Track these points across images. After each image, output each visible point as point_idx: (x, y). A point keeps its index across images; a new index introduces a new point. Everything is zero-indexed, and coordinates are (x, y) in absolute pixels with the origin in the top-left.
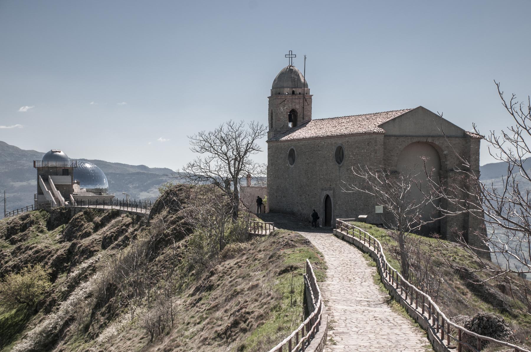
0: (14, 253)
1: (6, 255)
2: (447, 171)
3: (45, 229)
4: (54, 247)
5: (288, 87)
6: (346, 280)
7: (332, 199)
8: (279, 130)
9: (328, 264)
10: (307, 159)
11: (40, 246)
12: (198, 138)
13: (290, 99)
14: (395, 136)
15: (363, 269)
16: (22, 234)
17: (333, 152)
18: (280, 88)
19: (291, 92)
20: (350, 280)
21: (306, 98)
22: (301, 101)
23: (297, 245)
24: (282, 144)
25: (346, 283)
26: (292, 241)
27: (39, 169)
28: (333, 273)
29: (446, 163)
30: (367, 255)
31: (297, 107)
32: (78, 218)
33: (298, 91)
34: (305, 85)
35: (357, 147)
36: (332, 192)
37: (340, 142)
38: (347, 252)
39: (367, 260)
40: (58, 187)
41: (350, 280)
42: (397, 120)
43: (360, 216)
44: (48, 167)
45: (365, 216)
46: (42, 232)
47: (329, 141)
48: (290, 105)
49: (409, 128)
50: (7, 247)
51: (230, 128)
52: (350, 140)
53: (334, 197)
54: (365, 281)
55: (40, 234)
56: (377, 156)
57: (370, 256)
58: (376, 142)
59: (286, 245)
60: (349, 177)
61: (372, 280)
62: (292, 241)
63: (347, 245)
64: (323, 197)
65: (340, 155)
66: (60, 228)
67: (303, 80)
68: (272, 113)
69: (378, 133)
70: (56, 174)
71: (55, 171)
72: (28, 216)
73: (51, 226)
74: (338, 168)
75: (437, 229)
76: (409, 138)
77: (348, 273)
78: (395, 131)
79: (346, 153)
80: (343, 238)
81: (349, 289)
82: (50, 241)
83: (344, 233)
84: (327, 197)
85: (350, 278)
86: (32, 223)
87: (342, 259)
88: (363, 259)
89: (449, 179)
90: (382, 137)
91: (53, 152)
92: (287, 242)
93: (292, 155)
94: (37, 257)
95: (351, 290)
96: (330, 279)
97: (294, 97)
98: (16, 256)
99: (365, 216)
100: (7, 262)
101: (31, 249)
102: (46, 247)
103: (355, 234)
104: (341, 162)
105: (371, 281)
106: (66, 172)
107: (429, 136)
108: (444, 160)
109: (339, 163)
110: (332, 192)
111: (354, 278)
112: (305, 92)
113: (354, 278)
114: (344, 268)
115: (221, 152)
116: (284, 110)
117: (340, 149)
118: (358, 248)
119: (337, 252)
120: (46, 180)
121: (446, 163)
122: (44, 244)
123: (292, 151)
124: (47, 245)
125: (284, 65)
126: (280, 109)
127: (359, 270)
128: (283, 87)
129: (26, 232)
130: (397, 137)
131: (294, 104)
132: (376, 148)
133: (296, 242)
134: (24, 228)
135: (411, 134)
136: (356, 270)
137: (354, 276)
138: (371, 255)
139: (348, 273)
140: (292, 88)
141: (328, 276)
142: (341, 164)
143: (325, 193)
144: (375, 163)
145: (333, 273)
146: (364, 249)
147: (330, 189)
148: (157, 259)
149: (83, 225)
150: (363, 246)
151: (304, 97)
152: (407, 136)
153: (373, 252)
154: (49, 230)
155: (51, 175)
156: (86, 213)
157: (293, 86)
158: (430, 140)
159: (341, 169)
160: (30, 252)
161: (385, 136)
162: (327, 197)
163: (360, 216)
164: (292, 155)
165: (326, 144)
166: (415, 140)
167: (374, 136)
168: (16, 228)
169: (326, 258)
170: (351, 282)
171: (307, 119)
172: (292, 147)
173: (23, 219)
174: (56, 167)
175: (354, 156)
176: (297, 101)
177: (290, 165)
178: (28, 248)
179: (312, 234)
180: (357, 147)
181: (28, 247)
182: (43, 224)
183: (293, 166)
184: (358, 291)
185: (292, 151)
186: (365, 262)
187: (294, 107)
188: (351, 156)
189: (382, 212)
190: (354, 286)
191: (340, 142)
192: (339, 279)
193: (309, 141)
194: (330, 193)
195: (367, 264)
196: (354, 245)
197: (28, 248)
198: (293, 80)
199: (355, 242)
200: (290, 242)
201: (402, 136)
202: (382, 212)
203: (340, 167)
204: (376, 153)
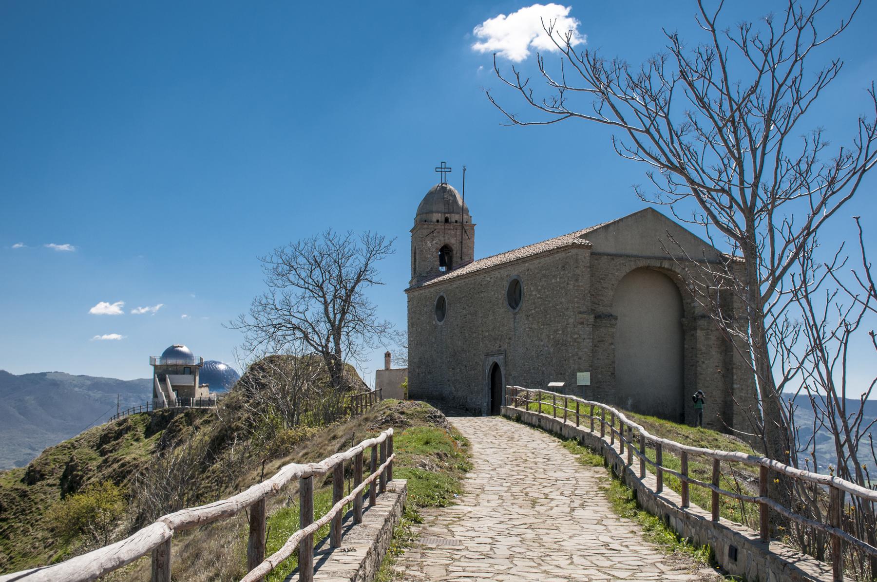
0: (99, 468)
1: (90, 470)
2: (695, 319)
3: (142, 436)
4: (143, 459)
5: (438, 212)
6: (520, 501)
7: (502, 369)
8: (425, 275)
9: (477, 461)
10: (464, 308)
11: (128, 458)
12: (275, 259)
13: (442, 230)
14: (608, 255)
15: (569, 472)
16: (115, 443)
17: (504, 292)
18: (426, 213)
19: (443, 220)
20: (534, 503)
21: (466, 228)
22: (459, 232)
23: (412, 422)
24: (427, 291)
25: (520, 511)
26: (402, 413)
27: (155, 366)
28: (485, 481)
29: (692, 305)
30: (572, 443)
31: (453, 241)
32: (176, 421)
33: (454, 217)
34: (464, 210)
35: (544, 276)
36: (502, 357)
37: (514, 272)
38: (525, 438)
39: (574, 452)
40: (175, 388)
41: (534, 503)
42: (611, 228)
43: (551, 384)
44: (167, 365)
45: (561, 384)
46: (137, 440)
47: (497, 274)
48: (442, 239)
49: (632, 243)
50: (95, 459)
51: (329, 243)
52: (531, 267)
53: (506, 363)
54: (582, 506)
55: (135, 443)
56: (579, 286)
57: (581, 443)
58: (577, 261)
59: (387, 422)
60: (531, 328)
61: (605, 502)
62: (402, 413)
63: (525, 430)
64: (488, 367)
65: (515, 294)
66: (157, 435)
67: (460, 203)
68: (415, 253)
69: (580, 246)
70: (176, 372)
71: (176, 370)
72: (125, 420)
73: (149, 433)
74: (512, 316)
75: (682, 410)
76: (633, 259)
77: (529, 481)
78: (607, 246)
79: (525, 288)
80: (519, 419)
81: (530, 535)
82: (142, 452)
83: (522, 409)
84: (495, 367)
85: (534, 494)
86: (128, 429)
87: (512, 450)
88: (565, 451)
89: (699, 331)
90: (587, 253)
91: (173, 347)
92: (390, 416)
93: (441, 307)
94: (122, 472)
95: (538, 540)
96: (470, 499)
97: (447, 226)
98: (100, 471)
99: (561, 384)
100: (89, 478)
101: (118, 461)
102: (134, 459)
103: (542, 410)
104: (517, 306)
105: (601, 507)
106: (189, 370)
107: (665, 259)
108: (689, 301)
109: (514, 308)
110: (502, 357)
111: (546, 496)
112: (465, 220)
113: (546, 496)
114: (516, 468)
115: (310, 281)
116: (432, 246)
117: (514, 286)
118: (550, 432)
119: (504, 440)
120: (163, 380)
121: (692, 305)
122: (133, 456)
123: (441, 300)
124: (137, 456)
125: (435, 183)
126: (426, 243)
127: (559, 475)
128: (432, 212)
129: (120, 440)
130: (613, 256)
131: (447, 236)
132: (578, 271)
133: (411, 416)
134: (119, 435)
135: (635, 253)
136: (551, 473)
137: (546, 490)
138: (583, 441)
139: (529, 481)
140: (445, 213)
141: (468, 488)
142: (516, 311)
143: (491, 360)
144: (576, 297)
145: (485, 481)
146: (565, 432)
147: (499, 353)
148: (211, 469)
149: (181, 430)
150: (563, 426)
151: (463, 228)
152: (628, 256)
153: (589, 434)
154: (146, 438)
155: (169, 373)
156: (187, 415)
157: (447, 211)
158: (666, 265)
159: (518, 316)
160: (116, 466)
161: (592, 254)
162: (495, 367)
163: (551, 384)
164: (441, 307)
165: (492, 280)
166: (642, 263)
167: (574, 251)
168: (110, 435)
169: (476, 448)
170: (538, 508)
171: (466, 259)
172: (442, 294)
173: (119, 424)
174: (176, 365)
175: (539, 291)
176: (452, 232)
177: (438, 323)
178: (116, 461)
179: (462, 418)
180: (544, 276)
181: (115, 459)
182: (141, 430)
183: (442, 323)
184: (569, 545)
185: (441, 300)
186: (572, 457)
187: (447, 241)
188: (534, 293)
189: (589, 384)
190: (549, 522)
191: (516, 273)
192: (501, 498)
193: (467, 280)
194: (499, 359)
195: (579, 460)
196: (542, 429)
197: (116, 461)
198: (446, 202)
199: (543, 423)
200: (396, 415)
201: (621, 256)
202: (589, 384)
203: (515, 314)
204: (577, 280)
